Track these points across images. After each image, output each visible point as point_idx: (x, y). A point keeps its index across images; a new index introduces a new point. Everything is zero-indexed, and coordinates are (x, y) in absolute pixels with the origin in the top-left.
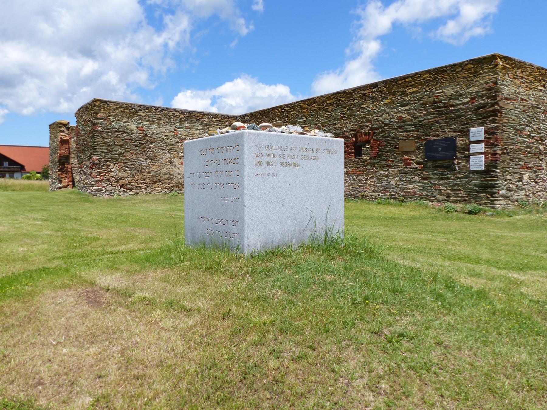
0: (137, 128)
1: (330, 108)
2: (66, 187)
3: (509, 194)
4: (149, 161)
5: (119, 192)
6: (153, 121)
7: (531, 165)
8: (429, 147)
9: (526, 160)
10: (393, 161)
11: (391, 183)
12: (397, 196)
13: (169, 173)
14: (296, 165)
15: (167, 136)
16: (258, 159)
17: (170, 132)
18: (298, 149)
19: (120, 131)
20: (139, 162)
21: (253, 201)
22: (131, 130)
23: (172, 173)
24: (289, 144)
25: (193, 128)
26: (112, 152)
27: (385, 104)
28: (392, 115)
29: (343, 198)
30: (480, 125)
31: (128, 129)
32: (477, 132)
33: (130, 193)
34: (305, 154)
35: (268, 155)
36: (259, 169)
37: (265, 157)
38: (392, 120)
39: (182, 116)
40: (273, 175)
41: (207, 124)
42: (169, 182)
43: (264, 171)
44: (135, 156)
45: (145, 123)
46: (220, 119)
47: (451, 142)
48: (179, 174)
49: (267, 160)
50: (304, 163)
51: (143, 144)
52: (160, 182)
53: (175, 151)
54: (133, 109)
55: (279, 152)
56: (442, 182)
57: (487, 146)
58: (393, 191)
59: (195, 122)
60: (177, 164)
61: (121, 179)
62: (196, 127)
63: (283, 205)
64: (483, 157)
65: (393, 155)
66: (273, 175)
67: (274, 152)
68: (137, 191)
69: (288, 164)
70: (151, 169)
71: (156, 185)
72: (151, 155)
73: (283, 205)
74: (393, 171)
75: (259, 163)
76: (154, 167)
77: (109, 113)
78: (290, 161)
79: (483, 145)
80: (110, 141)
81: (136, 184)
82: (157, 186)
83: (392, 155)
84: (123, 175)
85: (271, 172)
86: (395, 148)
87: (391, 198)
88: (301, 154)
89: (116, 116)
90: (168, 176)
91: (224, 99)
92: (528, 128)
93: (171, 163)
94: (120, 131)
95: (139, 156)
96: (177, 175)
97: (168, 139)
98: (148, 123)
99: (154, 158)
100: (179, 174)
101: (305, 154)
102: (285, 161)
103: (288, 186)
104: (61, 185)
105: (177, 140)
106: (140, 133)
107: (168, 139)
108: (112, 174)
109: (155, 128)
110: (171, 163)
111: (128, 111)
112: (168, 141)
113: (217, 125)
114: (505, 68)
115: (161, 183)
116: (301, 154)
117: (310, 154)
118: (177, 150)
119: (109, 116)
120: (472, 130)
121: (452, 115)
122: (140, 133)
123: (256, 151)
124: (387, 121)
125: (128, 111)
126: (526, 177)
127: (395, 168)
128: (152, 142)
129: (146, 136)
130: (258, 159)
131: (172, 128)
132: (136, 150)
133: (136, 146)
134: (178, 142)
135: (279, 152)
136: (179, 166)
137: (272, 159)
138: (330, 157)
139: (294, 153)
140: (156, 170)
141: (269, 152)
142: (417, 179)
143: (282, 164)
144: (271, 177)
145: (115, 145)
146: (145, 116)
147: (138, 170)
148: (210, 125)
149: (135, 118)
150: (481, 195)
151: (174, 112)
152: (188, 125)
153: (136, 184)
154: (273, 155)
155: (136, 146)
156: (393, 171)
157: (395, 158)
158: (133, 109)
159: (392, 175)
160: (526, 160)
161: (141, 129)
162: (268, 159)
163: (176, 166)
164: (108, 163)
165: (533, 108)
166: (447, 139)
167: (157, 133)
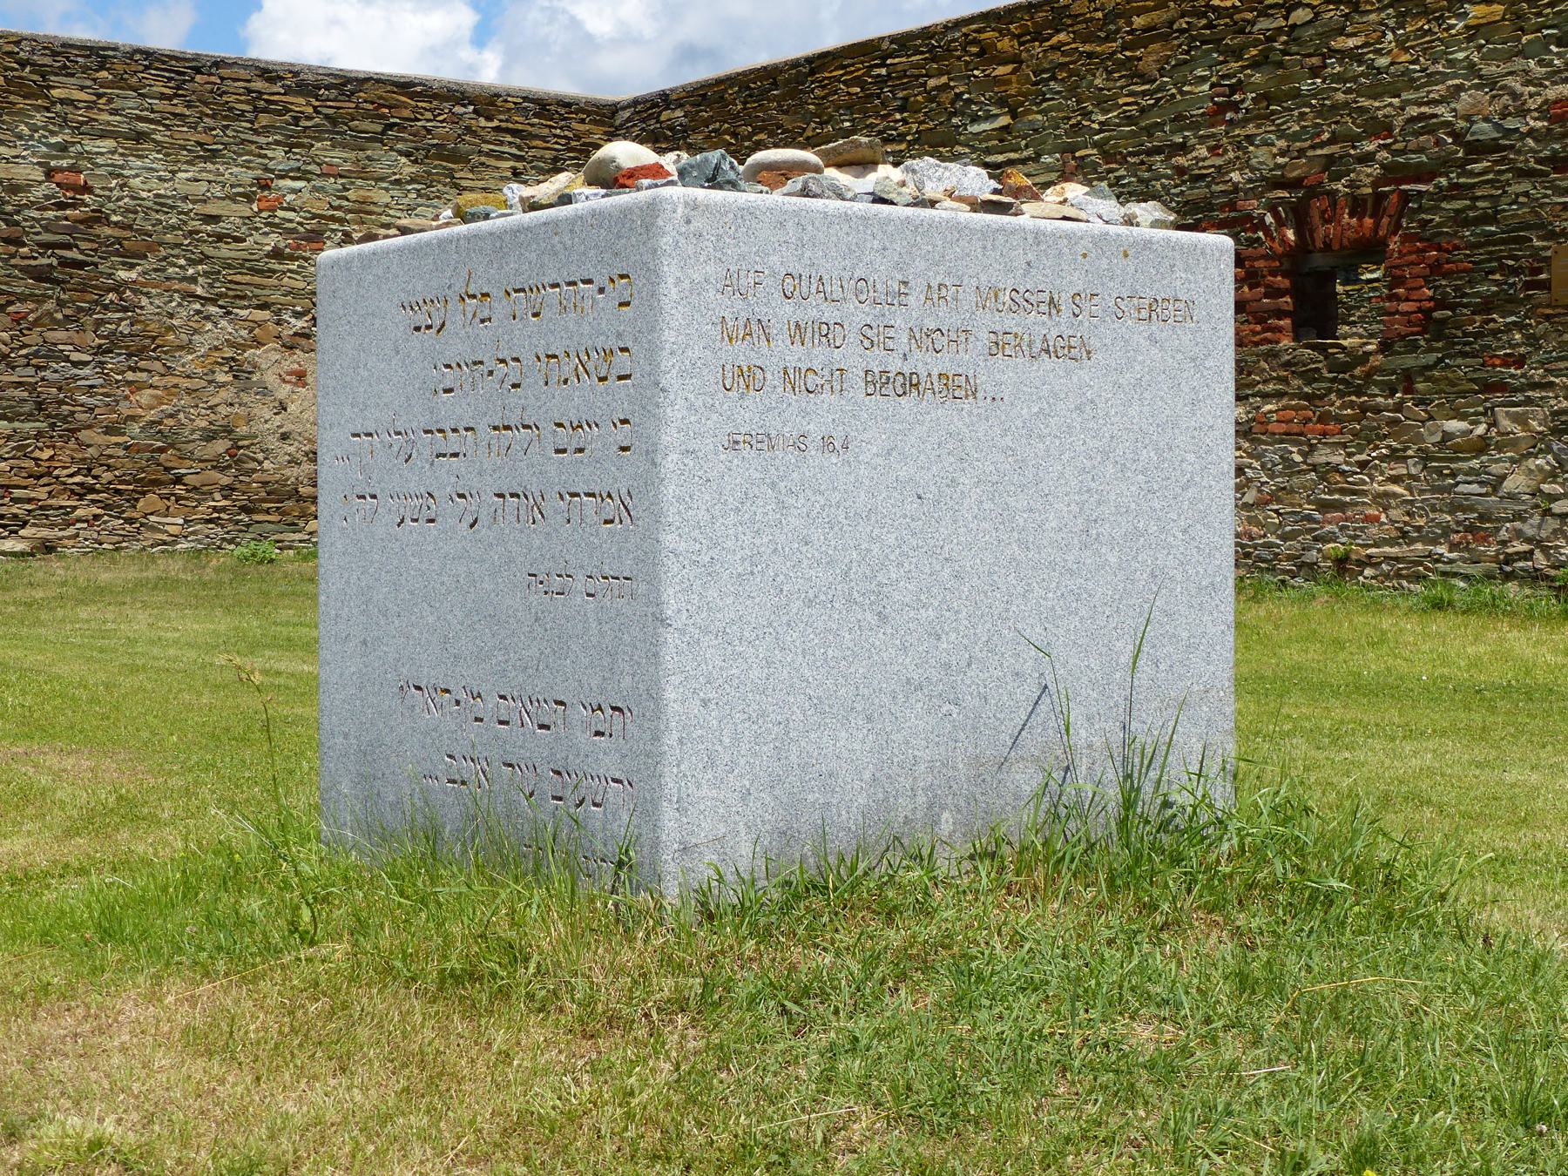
0: (50, 173)
4: (112, 362)
6: (140, 137)
10: (1520, 362)
11: (1508, 485)
12: (1540, 560)
13: (228, 431)
14: (954, 387)
15: (215, 219)
16: (742, 354)
23: (243, 430)
24: (920, 265)
25: (363, 174)
28: (1515, 96)
34: (1010, 322)
35: (798, 331)
36: (748, 413)
37: (781, 342)
38: (1510, 123)
39: (299, 103)
40: (827, 443)
43: (774, 424)
44: (33, 338)
45: (90, 145)
48: (285, 437)
50: (1006, 373)
51: (80, 265)
52: (178, 480)
54: (23, 64)
55: (857, 314)
58: (1519, 534)
59: (378, 139)
60: (271, 379)
62: (379, 169)
65: (1519, 326)
66: (827, 443)
67: (830, 314)
68: (45, 533)
69: (912, 384)
70: (124, 409)
71: (150, 501)
72: (124, 328)
74: (1521, 420)
75: (747, 378)
76: (145, 397)
78: (924, 363)
81: (41, 493)
82: (160, 505)
83: (1509, 328)
85: (815, 430)
86: (1528, 286)
87: (1508, 577)
88: (985, 323)
90: (221, 446)
93: (241, 373)
95: (60, 335)
96: (273, 443)
97: (220, 238)
98: (110, 143)
100: (285, 437)
102: (895, 364)
103: (912, 507)
105: (272, 241)
106: (61, 206)
107: (220, 238)
109: (147, 177)
115: (179, 490)
116: (985, 323)
117: (1037, 325)
122: (61, 206)
123: (730, 307)
127: (1529, 401)
129: (98, 218)
130: (742, 354)
131: (247, 176)
132: (40, 300)
133: (41, 275)
134: (276, 254)
135: (857, 314)
136: (283, 391)
137: (819, 356)
138: (1153, 340)
139: (945, 317)
140: (152, 415)
141: (799, 316)
143: (878, 382)
149: (39, 118)
151: (259, 85)
152: (338, 157)
153: (41, 493)
154: (825, 332)
156: (1516, 419)
157: (1532, 341)
158: (23, 64)
159: (1514, 443)
161: (70, 177)
162: (795, 356)
163: (265, 391)
167: (161, 204)
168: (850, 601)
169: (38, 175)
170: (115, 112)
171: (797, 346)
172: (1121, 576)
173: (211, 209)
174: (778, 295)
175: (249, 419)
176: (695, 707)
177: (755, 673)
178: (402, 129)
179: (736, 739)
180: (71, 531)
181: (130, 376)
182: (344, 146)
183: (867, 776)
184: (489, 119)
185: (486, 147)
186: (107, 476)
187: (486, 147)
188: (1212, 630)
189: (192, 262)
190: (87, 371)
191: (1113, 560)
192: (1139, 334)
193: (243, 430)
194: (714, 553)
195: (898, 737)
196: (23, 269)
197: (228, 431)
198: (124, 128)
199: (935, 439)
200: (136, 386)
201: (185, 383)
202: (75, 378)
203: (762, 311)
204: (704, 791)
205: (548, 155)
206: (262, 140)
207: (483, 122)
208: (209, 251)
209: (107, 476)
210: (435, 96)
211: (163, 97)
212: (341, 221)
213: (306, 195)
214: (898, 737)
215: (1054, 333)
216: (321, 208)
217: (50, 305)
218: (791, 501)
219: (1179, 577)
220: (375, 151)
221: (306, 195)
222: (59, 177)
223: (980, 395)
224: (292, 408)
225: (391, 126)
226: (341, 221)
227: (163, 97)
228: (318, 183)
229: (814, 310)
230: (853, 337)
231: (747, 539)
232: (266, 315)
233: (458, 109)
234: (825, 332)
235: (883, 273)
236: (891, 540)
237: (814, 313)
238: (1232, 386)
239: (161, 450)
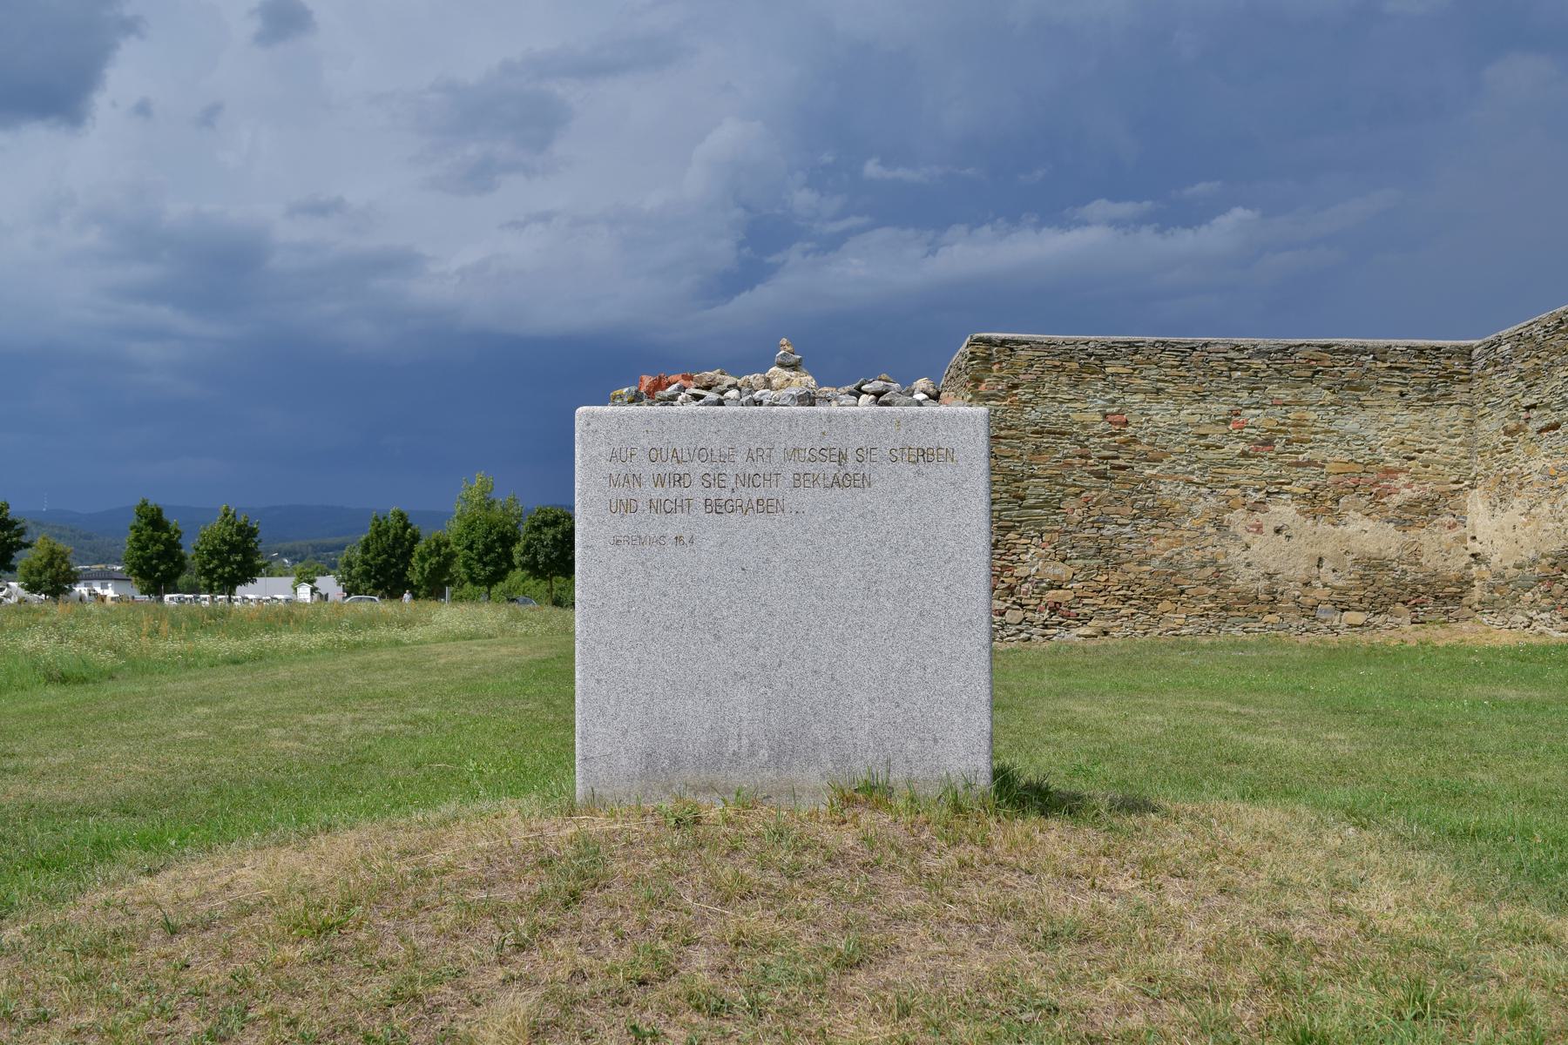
0: (1105, 416)
4: (1142, 523)
5: (1046, 627)
6: (1158, 391)
13: (1214, 561)
14: (764, 506)
15: (1205, 436)
16: (623, 493)
17: (1216, 423)
18: (778, 455)
19: (1049, 432)
21: (603, 622)
22: (1085, 427)
23: (1222, 561)
24: (743, 438)
25: (1299, 403)
26: (1023, 499)
29: (558, 609)
31: (1073, 424)
33: (1082, 631)
34: (809, 468)
35: (660, 481)
36: (626, 525)
37: (648, 486)
39: (1257, 363)
41: (1350, 385)
42: (1212, 591)
44: (1096, 511)
45: (1128, 398)
46: (1402, 361)
48: (1249, 565)
49: (655, 496)
51: (1124, 468)
52: (1182, 592)
53: (1236, 487)
54: (1090, 355)
55: (698, 468)
59: (1310, 380)
60: (1240, 530)
61: (1051, 587)
62: (1308, 398)
63: (717, 638)
67: (681, 469)
68: (1102, 624)
70: (1149, 550)
71: (1165, 605)
72: (1150, 503)
73: (717, 638)
75: (627, 507)
76: (1162, 543)
77: (1016, 375)
80: (1017, 466)
81: (1100, 601)
84: (1057, 571)
85: (671, 533)
88: (790, 469)
89: (1037, 383)
90: (1209, 571)
93: (1220, 526)
94: (1049, 432)
95: (1112, 509)
96: (1241, 568)
97: (1208, 447)
98: (1141, 396)
99: (1162, 514)
100: (1249, 565)
101: (809, 468)
103: (738, 575)
105: (1242, 446)
106: (1113, 435)
107: (1208, 447)
108: (1021, 571)
109: (1162, 414)
110: (1220, 526)
111: (1075, 365)
112: (1211, 454)
113: (1391, 384)
116: (790, 469)
118: (1243, 481)
119: (1015, 386)
122: (1113, 435)
123: (617, 468)
125: (1075, 365)
129: (1134, 440)
130: (623, 493)
131: (1225, 409)
132: (1100, 490)
133: (1101, 475)
134: (1244, 454)
135: (698, 468)
136: (1247, 538)
137: (674, 493)
139: (762, 467)
140: (1166, 554)
141: (660, 470)
143: (715, 507)
144: (670, 547)
145: (1032, 476)
146: (1129, 376)
148: (1366, 388)
149: (1100, 385)
151: (1232, 354)
152: (1284, 394)
153: (1100, 601)
154: (679, 480)
158: (1090, 355)
161: (1117, 418)
162: (658, 493)
163: (1236, 537)
164: (1012, 535)
167: (1172, 430)
168: (695, 627)
169: (1099, 418)
170: (1144, 378)
171: (659, 488)
172: (896, 615)
173: (1202, 431)
174: (646, 460)
175: (1226, 554)
176: (593, 684)
177: (631, 666)
178: (1325, 373)
179: (619, 702)
180: (1118, 622)
181: (1153, 531)
182: (1287, 387)
183: (707, 726)
184: (1384, 361)
185: (1381, 380)
186: (1140, 590)
187: (1381, 380)
188: (969, 649)
189: (1190, 463)
190: (1128, 529)
191: (888, 605)
192: (908, 470)
193: (1222, 561)
194: (605, 601)
195: (730, 705)
196: (1091, 473)
197: (1214, 561)
198: (1149, 387)
199: (754, 536)
200: (1157, 537)
201: (1187, 534)
202: (1120, 534)
203: (636, 470)
204: (598, 729)
205: (1425, 381)
206: (1234, 387)
207: (1379, 364)
208: (1201, 455)
209: (1140, 590)
210: (1347, 351)
211: (1172, 367)
212: (1285, 432)
213: (1262, 418)
214: (730, 705)
215: (843, 472)
216: (1272, 425)
217: (1105, 492)
218: (654, 572)
219: (942, 616)
220: (1307, 387)
221: (1262, 418)
222: (1110, 418)
223: (787, 510)
224: (1253, 547)
225: (1317, 372)
226: (1285, 432)
227: (1172, 367)
228: (1270, 410)
229: (670, 467)
230: (697, 481)
231: (626, 593)
232: (1237, 491)
233: (1363, 358)
234: (679, 480)
235: (717, 444)
236: (723, 594)
237: (671, 469)
238: (986, 499)
239: (1172, 574)
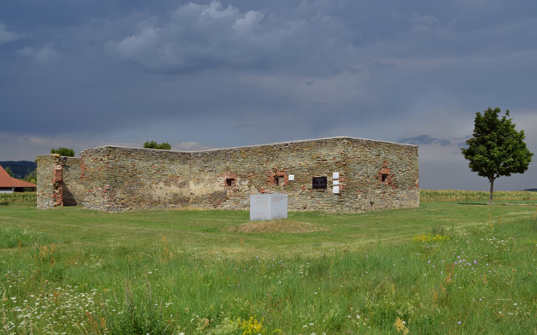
1: (260, 154)
2: (59, 205)
3: (351, 205)
4: (138, 186)
7: (363, 190)
8: (315, 180)
9: (359, 187)
20: (132, 188)
27: (292, 156)
30: (337, 171)
32: (336, 175)
39: (157, 154)
46: (180, 155)
47: (325, 178)
56: (321, 199)
57: (340, 182)
64: (338, 187)
79: (338, 181)
80: (116, 174)
89: (119, 157)
91: (27, 51)
92: (360, 172)
93: (151, 187)
99: (141, 185)
104: (56, 204)
108: (117, 196)
112: (149, 173)
114: (348, 143)
120: (334, 173)
121: (325, 165)
124: (293, 166)
126: (359, 196)
128: (140, 174)
133: (131, 176)
134: (155, 173)
142: (309, 198)
147: (131, 193)
150: (337, 205)
155: (131, 176)
160: (359, 187)
165: (364, 161)
166: (322, 177)
167: (143, 167)
